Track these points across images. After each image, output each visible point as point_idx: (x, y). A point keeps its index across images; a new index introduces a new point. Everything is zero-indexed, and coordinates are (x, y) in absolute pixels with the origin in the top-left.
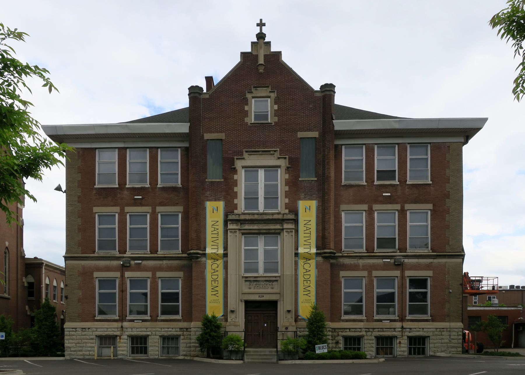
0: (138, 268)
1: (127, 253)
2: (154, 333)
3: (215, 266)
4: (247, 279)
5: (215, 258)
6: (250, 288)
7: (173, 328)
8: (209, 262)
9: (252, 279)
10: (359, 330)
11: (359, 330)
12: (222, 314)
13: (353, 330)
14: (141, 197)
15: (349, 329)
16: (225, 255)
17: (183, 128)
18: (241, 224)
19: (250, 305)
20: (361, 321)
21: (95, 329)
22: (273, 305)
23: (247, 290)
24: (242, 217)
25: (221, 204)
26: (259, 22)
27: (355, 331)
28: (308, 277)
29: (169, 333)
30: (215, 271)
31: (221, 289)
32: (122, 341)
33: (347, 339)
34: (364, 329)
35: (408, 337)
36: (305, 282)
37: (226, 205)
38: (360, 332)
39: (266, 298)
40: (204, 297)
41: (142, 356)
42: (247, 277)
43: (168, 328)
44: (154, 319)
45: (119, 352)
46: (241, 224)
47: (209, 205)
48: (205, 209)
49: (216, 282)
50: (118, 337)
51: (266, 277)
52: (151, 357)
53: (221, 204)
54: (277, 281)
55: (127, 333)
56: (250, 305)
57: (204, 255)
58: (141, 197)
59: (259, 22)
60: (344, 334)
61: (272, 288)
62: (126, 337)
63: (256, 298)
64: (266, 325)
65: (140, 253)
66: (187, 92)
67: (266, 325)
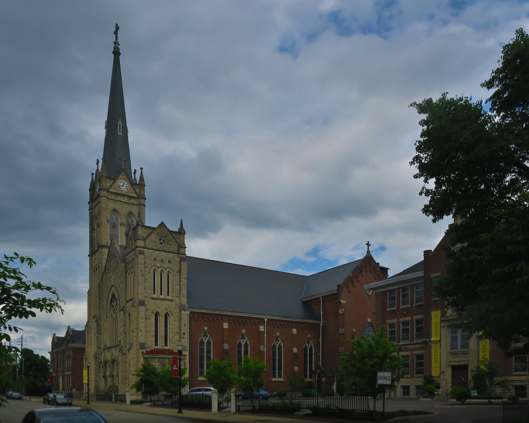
0: (406, 350)
1: (414, 341)
2: (412, 384)
3: (436, 347)
4: (452, 354)
5: (435, 342)
6: (454, 358)
7: (420, 382)
8: (433, 345)
9: (454, 353)
10: (523, 381)
11: (523, 381)
12: (439, 374)
13: (519, 381)
14: (406, 312)
15: (517, 381)
16: (440, 340)
17: (421, 274)
18: (448, 322)
19: (454, 368)
20: (525, 375)
21: (414, 382)
22: (465, 367)
23: (451, 359)
24: (450, 318)
25: (439, 312)
26: (367, 243)
27: (520, 382)
28: (485, 349)
29: (419, 384)
30: (436, 350)
31: (438, 360)
32: (398, 388)
33: (517, 387)
34: (527, 381)
35: (401, 386)
36: (483, 353)
37: (441, 312)
38: (524, 382)
39: (462, 363)
40: (431, 364)
41: (407, 397)
42: (451, 352)
43: (418, 382)
44: (412, 377)
45: (397, 395)
46: (448, 322)
47: (433, 313)
48: (431, 316)
49: (485, 353)
50: (396, 387)
51: (461, 351)
52: (411, 397)
53: (439, 312)
54: (467, 353)
55: (400, 385)
56: (454, 368)
57: (430, 341)
58: (406, 312)
59: (367, 243)
60: (513, 384)
61: (465, 358)
62: (400, 387)
63: (456, 364)
64: (464, 379)
65: (406, 342)
66: (423, 253)
67: (464, 379)
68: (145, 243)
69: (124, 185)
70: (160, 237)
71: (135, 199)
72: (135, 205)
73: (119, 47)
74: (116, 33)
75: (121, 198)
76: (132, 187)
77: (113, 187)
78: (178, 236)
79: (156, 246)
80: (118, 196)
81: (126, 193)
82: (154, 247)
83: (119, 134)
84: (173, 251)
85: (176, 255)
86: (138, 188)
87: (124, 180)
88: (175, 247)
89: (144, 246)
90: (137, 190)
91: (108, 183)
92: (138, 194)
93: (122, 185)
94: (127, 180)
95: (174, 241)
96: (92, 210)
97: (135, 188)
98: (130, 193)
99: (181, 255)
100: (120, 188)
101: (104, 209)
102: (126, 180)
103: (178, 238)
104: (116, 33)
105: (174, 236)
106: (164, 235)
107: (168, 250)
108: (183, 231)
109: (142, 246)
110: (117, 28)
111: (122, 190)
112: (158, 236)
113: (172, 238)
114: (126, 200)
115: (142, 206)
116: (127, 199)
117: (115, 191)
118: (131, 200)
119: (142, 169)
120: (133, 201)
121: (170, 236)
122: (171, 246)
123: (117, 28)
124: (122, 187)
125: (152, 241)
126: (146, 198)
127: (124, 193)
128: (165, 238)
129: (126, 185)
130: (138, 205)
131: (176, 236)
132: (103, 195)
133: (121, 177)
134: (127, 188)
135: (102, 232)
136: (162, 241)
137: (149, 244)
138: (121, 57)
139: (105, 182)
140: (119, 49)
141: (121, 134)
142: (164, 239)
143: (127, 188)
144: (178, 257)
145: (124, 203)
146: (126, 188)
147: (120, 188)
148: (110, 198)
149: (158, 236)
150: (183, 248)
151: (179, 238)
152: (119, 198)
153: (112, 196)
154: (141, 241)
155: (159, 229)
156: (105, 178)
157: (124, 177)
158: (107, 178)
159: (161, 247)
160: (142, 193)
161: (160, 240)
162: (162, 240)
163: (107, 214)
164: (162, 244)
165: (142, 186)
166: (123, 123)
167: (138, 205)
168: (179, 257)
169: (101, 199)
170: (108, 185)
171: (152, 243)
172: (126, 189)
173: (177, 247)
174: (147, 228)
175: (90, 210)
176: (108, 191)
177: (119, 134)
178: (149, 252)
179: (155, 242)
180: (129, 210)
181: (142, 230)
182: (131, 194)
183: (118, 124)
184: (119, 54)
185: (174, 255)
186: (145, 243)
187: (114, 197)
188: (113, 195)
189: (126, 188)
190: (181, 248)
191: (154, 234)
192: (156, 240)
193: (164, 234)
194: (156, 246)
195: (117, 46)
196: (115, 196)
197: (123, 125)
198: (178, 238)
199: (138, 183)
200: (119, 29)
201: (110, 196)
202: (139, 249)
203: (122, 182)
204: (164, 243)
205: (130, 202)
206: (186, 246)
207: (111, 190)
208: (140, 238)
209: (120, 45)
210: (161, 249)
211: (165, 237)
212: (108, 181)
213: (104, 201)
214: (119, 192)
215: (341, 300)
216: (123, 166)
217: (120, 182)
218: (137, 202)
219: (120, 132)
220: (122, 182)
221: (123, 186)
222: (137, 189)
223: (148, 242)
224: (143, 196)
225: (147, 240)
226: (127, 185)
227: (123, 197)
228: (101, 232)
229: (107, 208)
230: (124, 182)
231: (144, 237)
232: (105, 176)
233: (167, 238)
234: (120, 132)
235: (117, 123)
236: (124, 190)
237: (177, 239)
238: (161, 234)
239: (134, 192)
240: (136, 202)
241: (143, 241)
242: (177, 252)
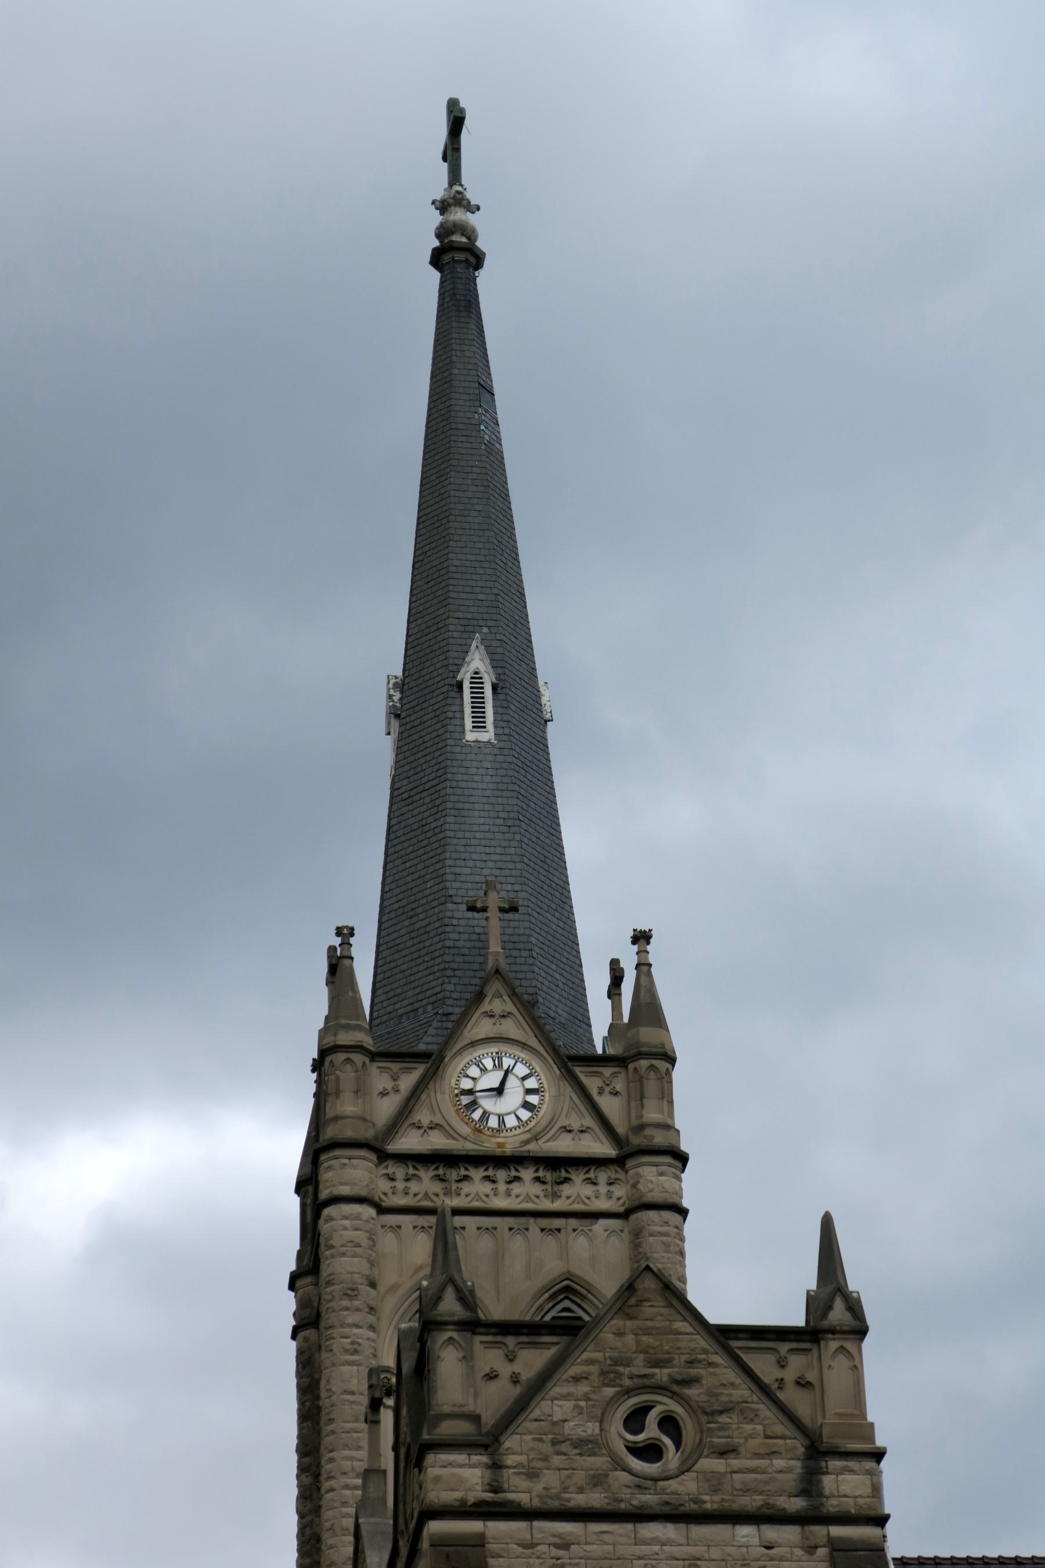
68: (496, 1466)
69: (512, 1082)
70: (628, 1392)
71: (603, 1176)
72: (602, 1222)
73: (472, 219)
74: (452, 153)
75: (487, 1188)
76: (568, 1091)
77: (423, 1116)
78: (797, 1364)
79: (598, 1480)
80: (466, 1178)
81: (527, 1142)
82: (581, 1490)
83: (470, 736)
84: (750, 1502)
85: (789, 1533)
86: (619, 1085)
87: (504, 1047)
88: (779, 1463)
89: (489, 1496)
90: (610, 1106)
91: (384, 1094)
92: (621, 1129)
93: (496, 1085)
94: (533, 1042)
95: (766, 1411)
96: (310, 1333)
97: (594, 1093)
98: (552, 1138)
99: (836, 1531)
100: (477, 1115)
101: (351, 1293)
102: (524, 1046)
103: (803, 1384)
104: (452, 153)
105: (763, 1365)
106: (662, 1375)
107: (711, 1503)
108: (838, 1314)
109: (472, 1498)
110: (456, 123)
111: (493, 1122)
112: (609, 1391)
113: (743, 1391)
114: (528, 1198)
115: (652, 1214)
116: (537, 1189)
117: (437, 1142)
118: (566, 1190)
119: (641, 938)
120: (588, 1190)
121: (729, 1373)
122: (736, 1463)
123: (456, 123)
124: (488, 1104)
125: (554, 1443)
126: (684, 1147)
127: (511, 1144)
128: (674, 1395)
129: (524, 1079)
130: (625, 1215)
131: (782, 1364)
132: (345, 1190)
133: (480, 1027)
134: (534, 1099)
135: (332, 1483)
136: (651, 1430)
137: (532, 1475)
138: (484, 280)
139: (360, 1091)
140: (471, 234)
141: (488, 735)
142: (667, 1404)
143: (534, 1099)
144: (811, 1549)
145: (510, 1221)
146: (526, 1105)
147: (477, 1115)
148: (401, 1201)
149: (609, 1391)
150: (852, 1464)
151: (811, 1376)
152: (466, 1188)
153: (414, 1186)
154: (461, 1458)
155: (620, 1334)
156: (358, 1058)
157: (510, 1028)
158: (374, 1056)
159: (643, 1483)
160: (652, 1115)
161: (635, 1420)
162: (652, 1418)
163: (372, 1328)
164: (651, 1452)
165: (644, 1063)
166: (497, 664)
167: (625, 1215)
168: (822, 1552)
169: (330, 1219)
170: (385, 1109)
171: (557, 1460)
172: (525, 1115)
173: (797, 1465)
174: (511, 1341)
175: (301, 1335)
176: (383, 1156)
177: (470, 736)
178: (532, 1545)
179: (585, 1445)
180: (552, 1267)
181: (467, 1358)
182: (563, 1146)
183: (465, 676)
184: (477, 259)
185: (771, 1532)
186: (496, 1466)
187: (437, 1187)
188: (422, 1173)
189: (526, 1105)
190: (835, 1464)
191: (577, 1379)
192: (592, 1428)
193: (658, 1364)
194: (598, 1480)
195: (458, 215)
196: (441, 1179)
197: (498, 676)
198: (803, 1384)
199: (600, 1051)
200: (467, 122)
201: (400, 1185)
202: (435, 1527)
203: (488, 1063)
204: (667, 1441)
205: (557, 1205)
206: (881, 1441)
207: (409, 1142)
208: (448, 1429)
209: (478, 208)
210: (650, 1499)
211: (673, 1388)
212: (379, 1078)
213: (350, 1234)
214: (469, 1147)
215: (591, 1041)
216: (495, 946)
217: (474, 1071)
218: (619, 1191)
219: (479, 725)
220: (488, 1063)
221: (499, 1091)
222: (616, 1094)
223: (522, 1459)
224: (659, 1139)
225: (510, 1442)
226: (531, 1084)
227: (501, 1175)
228: (330, 1478)
229: (373, 1285)
230: (507, 1062)
231: (382, 1408)
232: (359, 1048)
233: (692, 1392)
234: (479, 725)
235: (459, 666)
236: (511, 1122)
237: (790, 1396)
238: (639, 1367)
239: (589, 1121)
240: (609, 1195)
241: (475, 1458)
242: (797, 1504)
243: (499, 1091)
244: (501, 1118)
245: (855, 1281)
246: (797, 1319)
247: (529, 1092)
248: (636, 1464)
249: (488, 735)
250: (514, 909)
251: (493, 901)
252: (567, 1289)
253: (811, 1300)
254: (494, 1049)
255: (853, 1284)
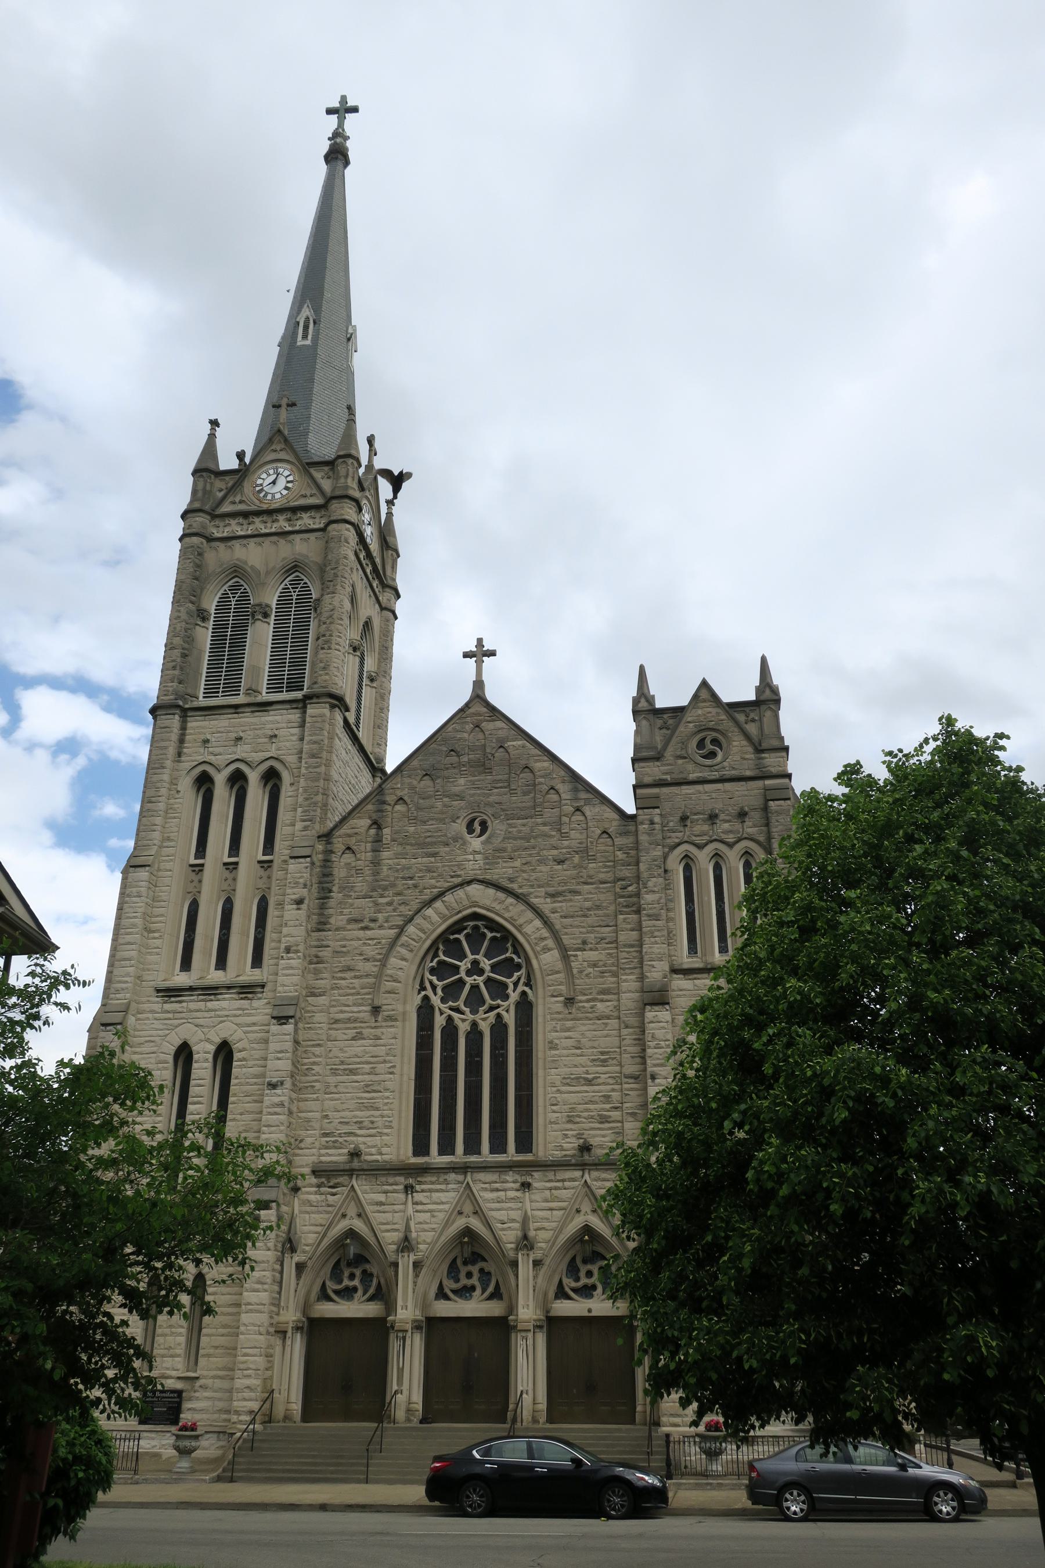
117: (242, 507)
130: (323, 530)
134: (290, 485)
143: (290, 485)
146: (286, 488)
162: (708, 741)
172: (285, 492)
207: (226, 508)
220: (271, 471)
221: (274, 482)
239: (314, 491)
243: (274, 482)
244: (273, 495)
245: (776, 680)
246: (752, 697)
247: (288, 482)
248: (708, 762)
249: (308, 342)
250: (293, 405)
251: (284, 402)
252: (296, 566)
253: (758, 689)
254: (274, 465)
255: (776, 681)
